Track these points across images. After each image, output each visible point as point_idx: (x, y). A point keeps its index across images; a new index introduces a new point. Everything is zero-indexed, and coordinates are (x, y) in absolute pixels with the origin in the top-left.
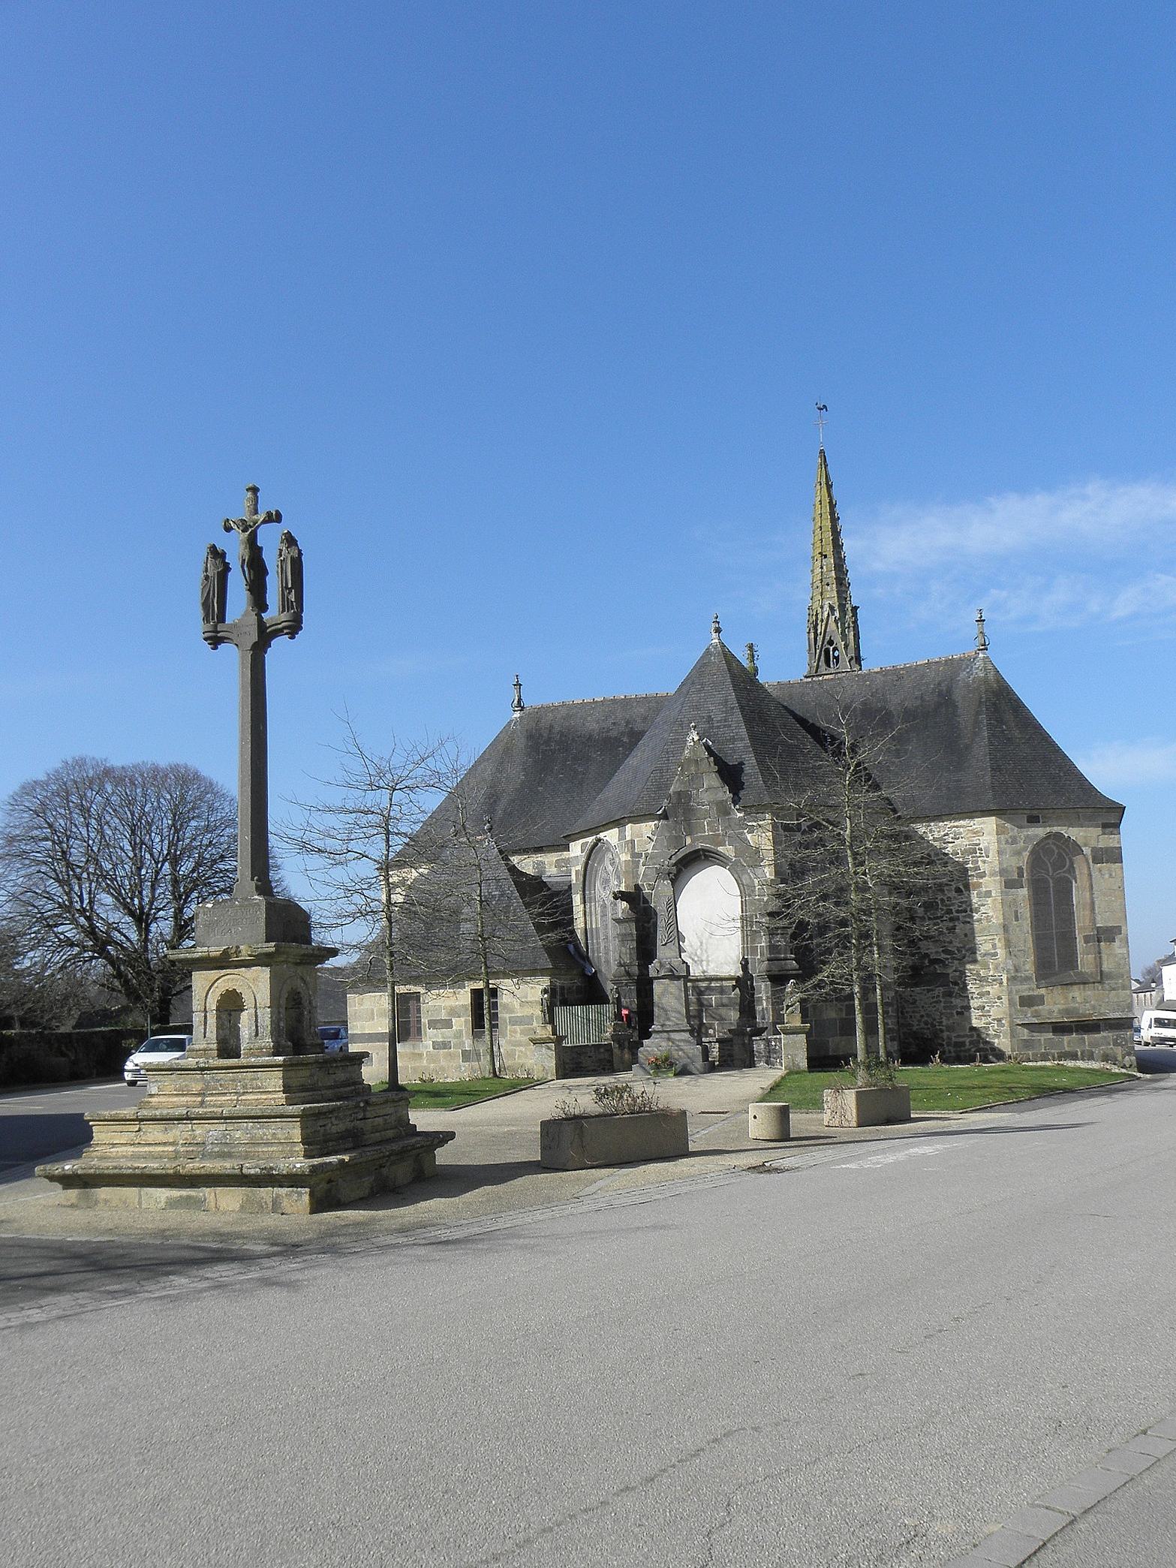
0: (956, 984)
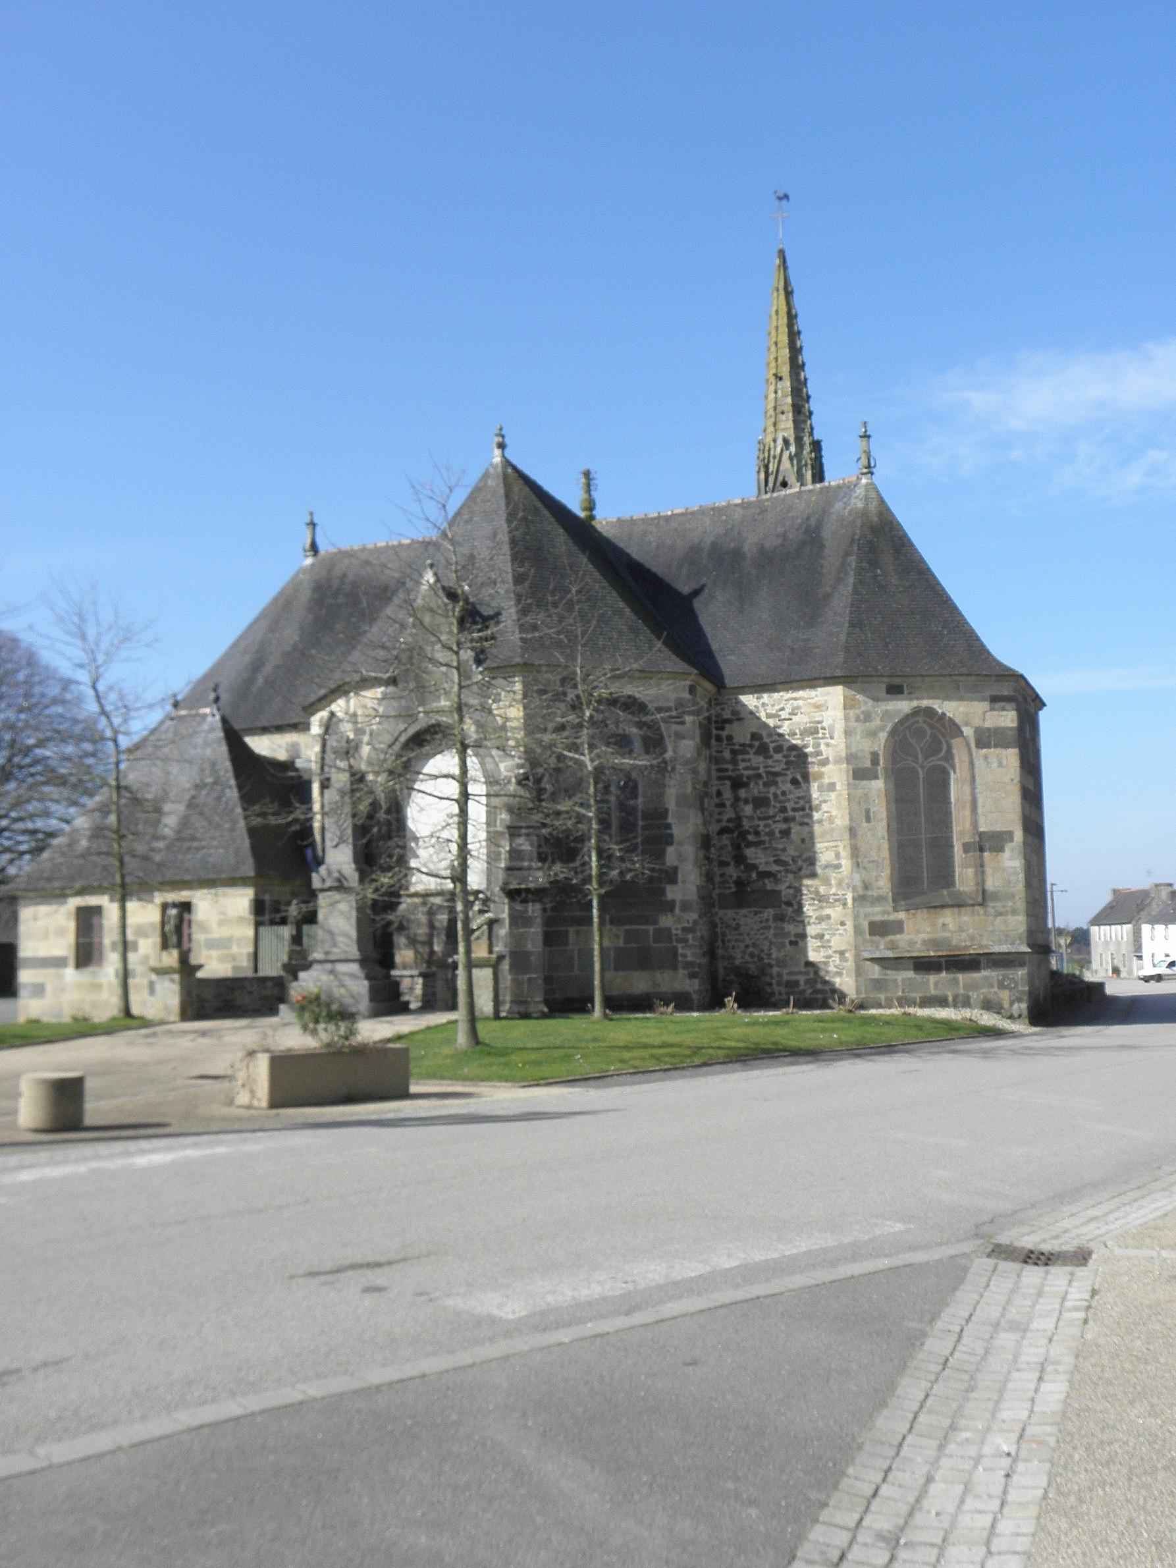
0: (789, 904)
